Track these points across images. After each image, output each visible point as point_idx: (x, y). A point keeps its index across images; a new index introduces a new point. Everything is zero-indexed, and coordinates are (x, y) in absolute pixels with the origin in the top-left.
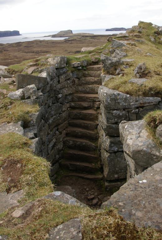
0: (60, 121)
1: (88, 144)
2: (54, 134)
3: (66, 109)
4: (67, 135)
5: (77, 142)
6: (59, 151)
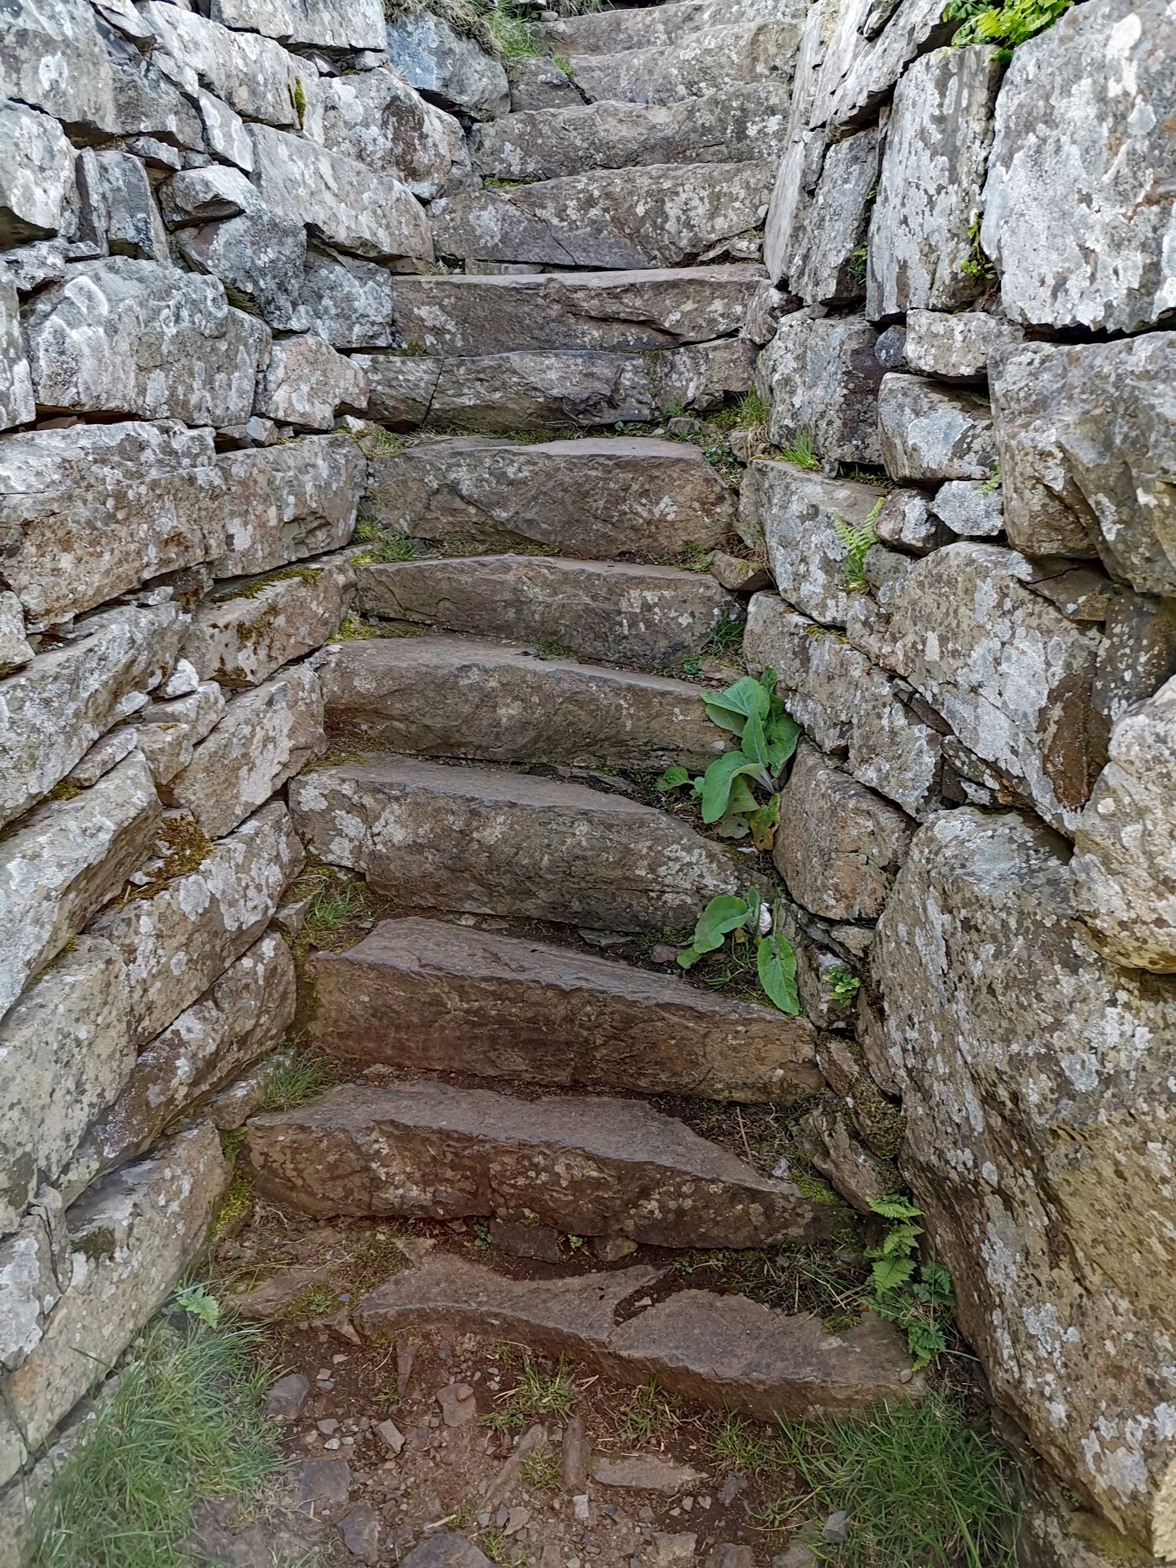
0: (242, 542)
1: (494, 832)
2: (137, 700)
3: (322, 413)
4: (343, 727)
5: (475, 812)
6: (218, 950)
